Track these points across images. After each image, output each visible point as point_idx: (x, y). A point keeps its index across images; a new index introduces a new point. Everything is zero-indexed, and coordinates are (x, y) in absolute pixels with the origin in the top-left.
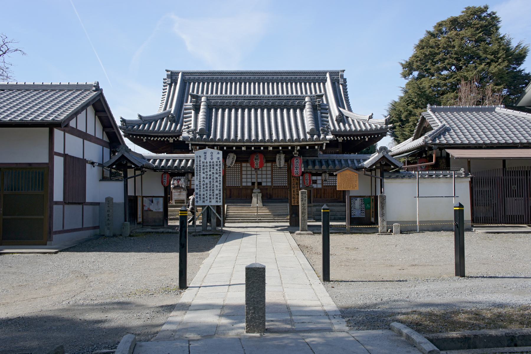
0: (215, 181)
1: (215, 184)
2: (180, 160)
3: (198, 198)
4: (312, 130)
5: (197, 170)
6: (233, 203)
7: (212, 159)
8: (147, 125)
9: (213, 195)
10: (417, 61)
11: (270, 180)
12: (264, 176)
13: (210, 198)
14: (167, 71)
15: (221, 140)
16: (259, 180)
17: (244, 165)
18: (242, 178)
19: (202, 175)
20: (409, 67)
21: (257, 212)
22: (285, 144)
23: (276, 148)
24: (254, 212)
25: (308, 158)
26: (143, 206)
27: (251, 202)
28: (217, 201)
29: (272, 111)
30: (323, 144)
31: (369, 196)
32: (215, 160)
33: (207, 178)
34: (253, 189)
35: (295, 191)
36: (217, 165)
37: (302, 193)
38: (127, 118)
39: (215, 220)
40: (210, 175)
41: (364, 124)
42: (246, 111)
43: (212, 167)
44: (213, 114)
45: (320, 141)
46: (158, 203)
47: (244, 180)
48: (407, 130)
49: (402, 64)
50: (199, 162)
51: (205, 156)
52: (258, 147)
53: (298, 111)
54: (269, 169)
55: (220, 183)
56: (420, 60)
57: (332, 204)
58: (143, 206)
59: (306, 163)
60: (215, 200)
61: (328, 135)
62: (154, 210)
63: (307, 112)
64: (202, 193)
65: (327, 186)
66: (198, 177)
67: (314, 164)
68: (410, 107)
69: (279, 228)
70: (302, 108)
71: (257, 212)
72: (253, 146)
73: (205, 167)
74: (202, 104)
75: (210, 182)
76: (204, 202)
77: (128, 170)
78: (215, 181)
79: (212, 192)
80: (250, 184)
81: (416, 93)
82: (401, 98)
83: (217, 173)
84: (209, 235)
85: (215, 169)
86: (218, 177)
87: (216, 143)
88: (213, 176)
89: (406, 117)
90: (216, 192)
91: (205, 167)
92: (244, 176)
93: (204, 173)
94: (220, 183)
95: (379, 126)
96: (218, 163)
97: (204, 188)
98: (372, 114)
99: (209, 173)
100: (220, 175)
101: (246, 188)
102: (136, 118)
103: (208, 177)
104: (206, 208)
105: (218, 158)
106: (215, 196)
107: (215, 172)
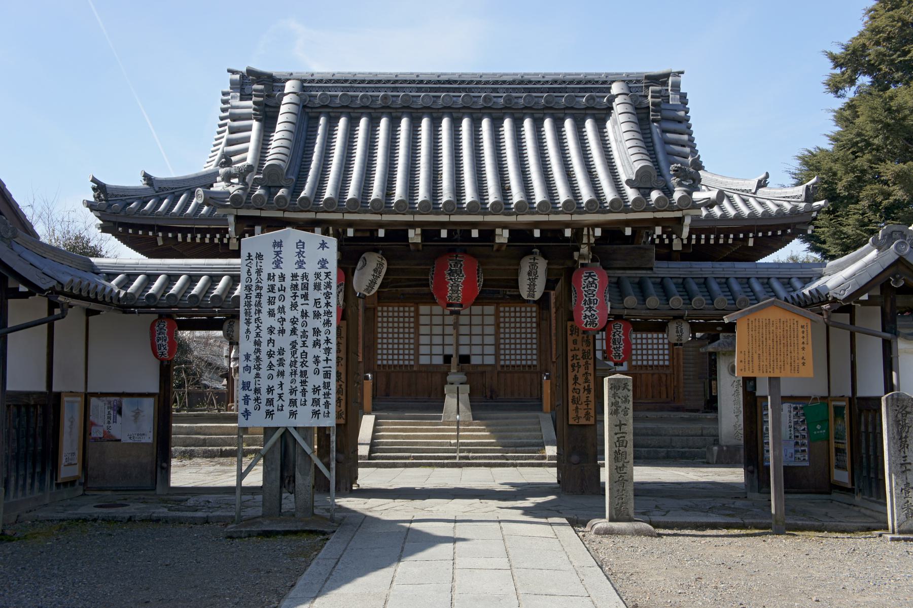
0: (310, 342)
1: (312, 352)
2: (211, 276)
3: (252, 403)
4: (641, 173)
5: (248, 304)
6: (395, 409)
7: (301, 264)
8: (166, 201)
9: (304, 392)
10: (877, 43)
11: (490, 350)
12: (477, 340)
13: (293, 402)
14: (233, 72)
15: (337, 202)
16: (464, 351)
17: (424, 309)
18: (417, 345)
19: (267, 321)
20: (852, 61)
21: (458, 437)
22: (553, 218)
23: (520, 234)
24: (450, 437)
25: (619, 273)
26: (87, 424)
27: (440, 408)
28: (316, 413)
29: (507, 124)
30: (680, 220)
31: (823, 398)
32: (311, 267)
33: (282, 331)
34: (446, 374)
35: (581, 380)
36: (317, 287)
37: (614, 386)
38: (110, 181)
39: (310, 480)
40: (294, 321)
41: (745, 202)
42: (425, 123)
43: (300, 293)
44: (320, 130)
45: (672, 208)
46: (137, 414)
47: (423, 350)
48: (851, 221)
49: (833, 58)
50: (254, 276)
51: (278, 253)
52: (460, 232)
53: (589, 125)
54: (490, 320)
55: (328, 350)
56: (888, 39)
57: (660, 414)
58: (87, 424)
59: (617, 288)
60: (309, 408)
61: (698, 190)
62: (125, 439)
63: (619, 128)
64: (264, 384)
65: (641, 367)
66: (253, 326)
67: (643, 294)
68: (862, 161)
69: (530, 502)
70: (602, 115)
71: (458, 437)
72: (443, 224)
73: (277, 294)
74: (286, 99)
75: (294, 344)
76: (269, 414)
77: (11, 302)
78: (310, 342)
79: (298, 379)
80: (439, 360)
81: (881, 121)
82: (835, 139)
83: (317, 315)
84: (286, 533)
85: (311, 302)
86: (323, 329)
87: (321, 216)
88: (305, 324)
89: (849, 187)
90: (316, 380)
91: (277, 294)
92: (424, 340)
93: (271, 313)
94: (328, 350)
95: (788, 207)
96: (323, 280)
97: (271, 366)
98: (767, 176)
99: (289, 314)
100: (327, 323)
101: (430, 370)
102: (138, 182)
103: (288, 326)
104: (277, 435)
105: (323, 263)
106: (310, 396)
107: (310, 309)
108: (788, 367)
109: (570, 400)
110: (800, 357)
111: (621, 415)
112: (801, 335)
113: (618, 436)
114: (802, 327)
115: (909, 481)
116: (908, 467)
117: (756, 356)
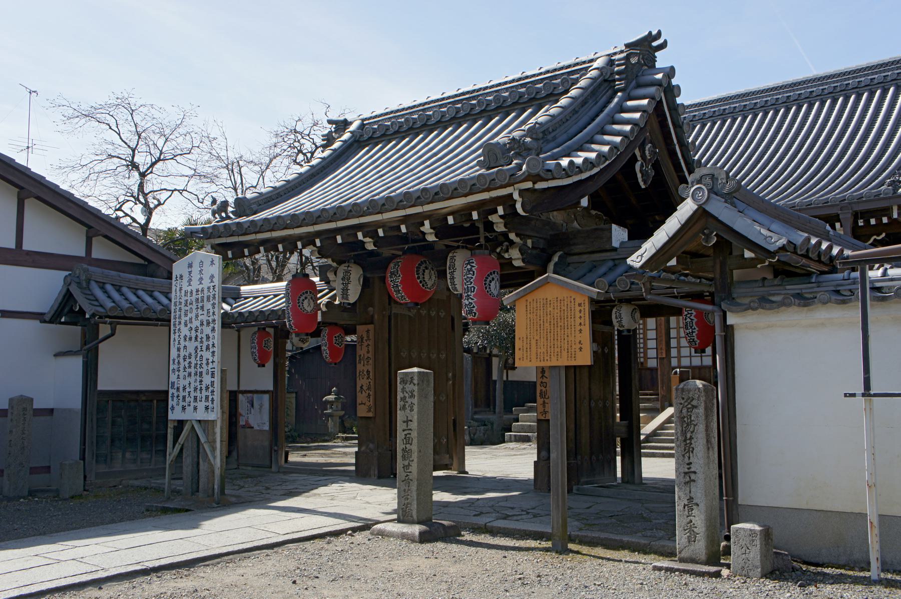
100: (213, 330)
108: (565, 354)
109: (538, 394)
110: (577, 341)
111: (408, 411)
112: (578, 315)
113: (406, 432)
114: (580, 305)
115: (692, 495)
116: (693, 477)
117: (533, 342)
